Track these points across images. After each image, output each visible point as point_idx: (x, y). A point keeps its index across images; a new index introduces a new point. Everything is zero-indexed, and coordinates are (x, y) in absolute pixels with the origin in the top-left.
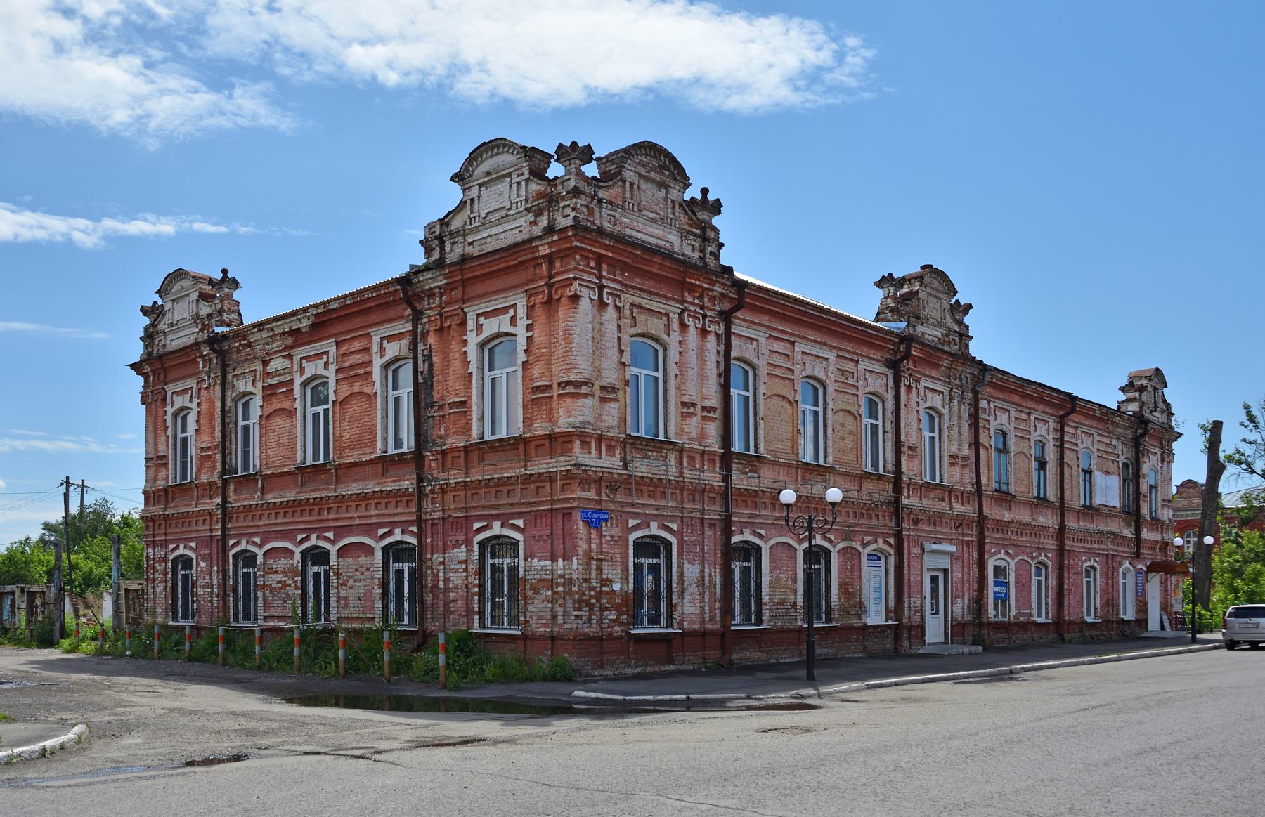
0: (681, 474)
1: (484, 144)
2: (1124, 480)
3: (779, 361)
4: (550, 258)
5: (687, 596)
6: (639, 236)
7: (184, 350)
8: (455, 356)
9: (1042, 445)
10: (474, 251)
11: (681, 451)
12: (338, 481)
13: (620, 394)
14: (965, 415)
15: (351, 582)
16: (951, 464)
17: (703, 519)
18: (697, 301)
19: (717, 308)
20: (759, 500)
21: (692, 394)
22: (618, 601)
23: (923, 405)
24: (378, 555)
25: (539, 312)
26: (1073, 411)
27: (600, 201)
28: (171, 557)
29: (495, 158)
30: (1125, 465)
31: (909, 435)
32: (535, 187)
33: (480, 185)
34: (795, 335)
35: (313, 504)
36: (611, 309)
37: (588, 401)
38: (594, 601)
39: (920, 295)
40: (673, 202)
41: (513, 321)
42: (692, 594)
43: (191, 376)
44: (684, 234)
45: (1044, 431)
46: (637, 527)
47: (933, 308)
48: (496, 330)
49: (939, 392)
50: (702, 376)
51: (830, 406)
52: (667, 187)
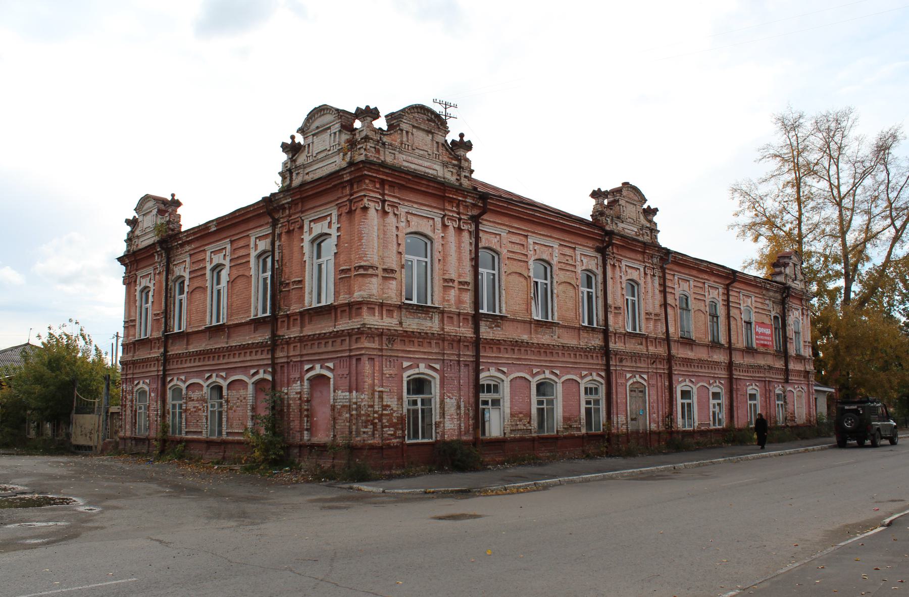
0: (443, 329)
3: (517, 249)
6: (413, 166)
8: (296, 249)
9: (714, 305)
10: (308, 178)
13: (397, 275)
17: (459, 361)
18: (454, 209)
19: (470, 214)
20: (502, 347)
22: (395, 421)
23: (624, 278)
24: (251, 388)
25: (344, 218)
26: (734, 281)
27: (384, 144)
28: (135, 390)
30: (775, 317)
32: (345, 136)
33: (313, 135)
34: (528, 231)
36: (391, 215)
37: (374, 280)
38: (376, 421)
39: (620, 202)
40: (437, 143)
42: (451, 415)
43: (151, 265)
44: (445, 165)
45: (715, 294)
46: (410, 367)
47: (630, 211)
50: (460, 260)
51: (555, 282)
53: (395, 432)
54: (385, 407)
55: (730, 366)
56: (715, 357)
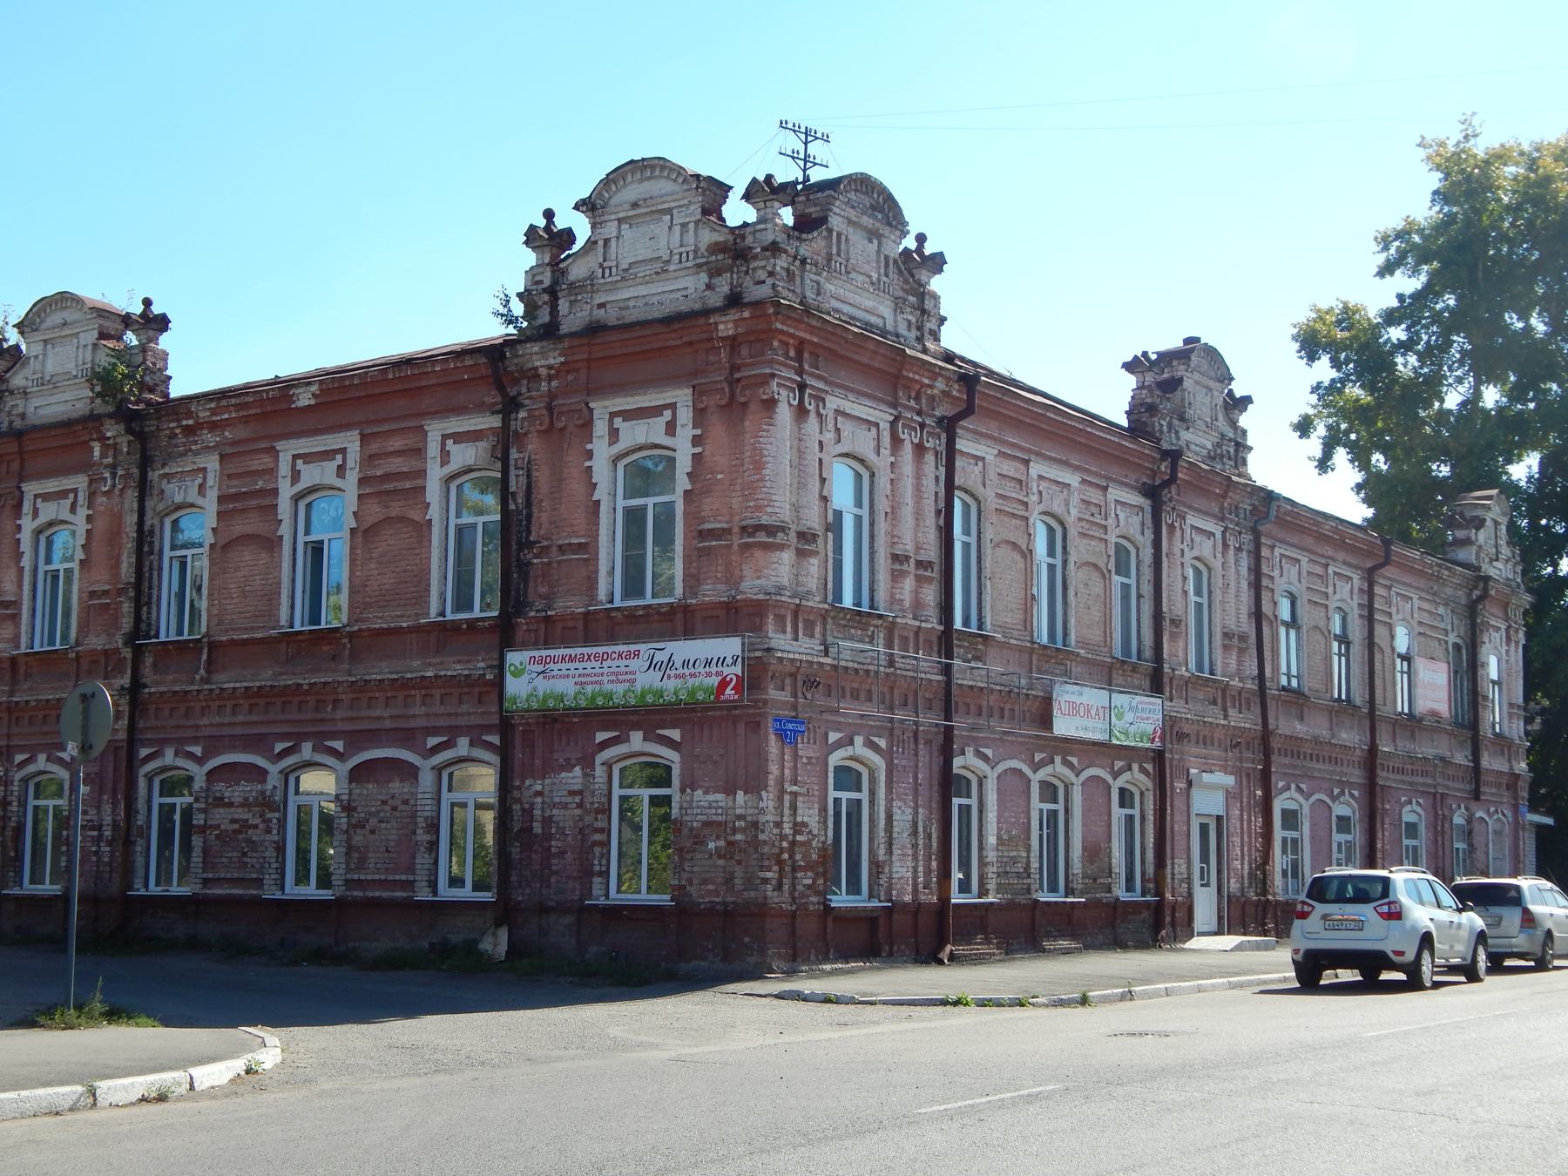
1: (632, 162)
2: (1456, 672)
4: (733, 342)
5: (896, 852)
7: (66, 425)
10: (610, 316)
11: (891, 628)
12: (355, 657)
14: (1244, 570)
15: (373, 822)
16: (1226, 648)
18: (913, 403)
21: (907, 546)
23: (1188, 554)
28: (18, 776)
29: (646, 184)
31: (1173, 603)
33: (620, 221)
34: (1029, 451)
35: (307, 693)
41: (671, 428)
46: (839, 745)
47: (1199, 397)
48: (641, 440)
49: (1211, 534)
50: (918, 515)
51: (1072, 559)
52: (879, 236)
53: (814, 881)
54: (798, 827)
55: (1371, 758)
56: (1344, 735)
